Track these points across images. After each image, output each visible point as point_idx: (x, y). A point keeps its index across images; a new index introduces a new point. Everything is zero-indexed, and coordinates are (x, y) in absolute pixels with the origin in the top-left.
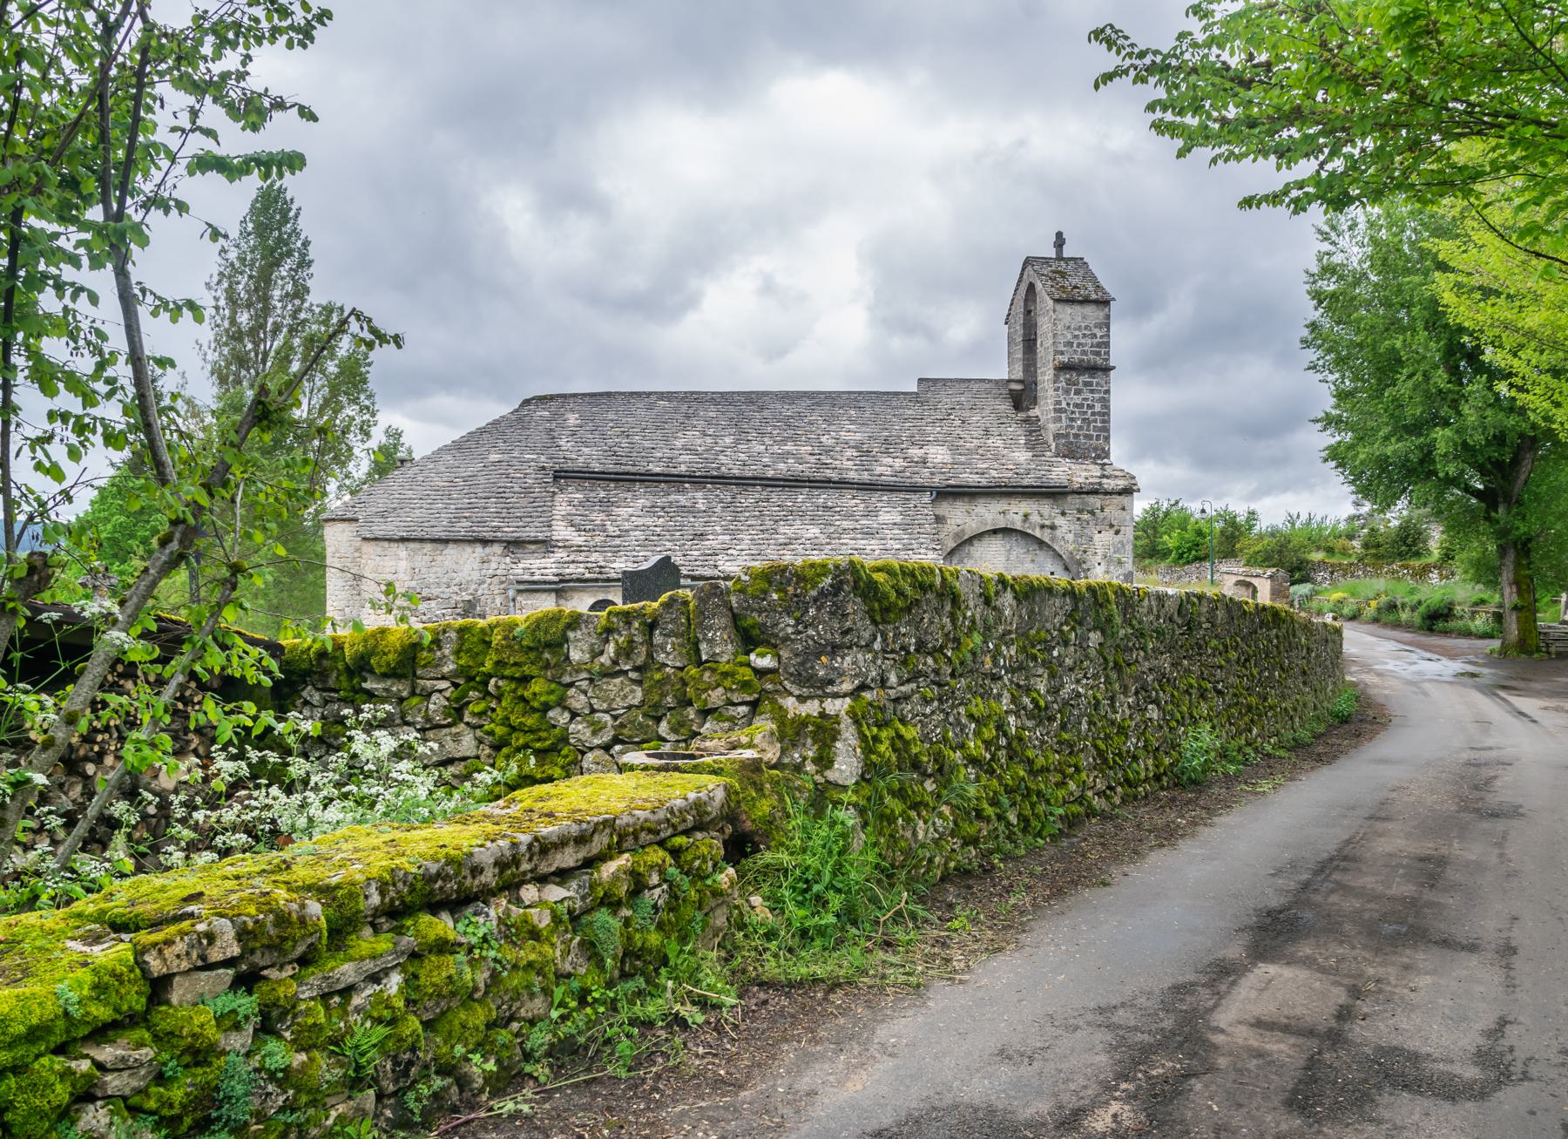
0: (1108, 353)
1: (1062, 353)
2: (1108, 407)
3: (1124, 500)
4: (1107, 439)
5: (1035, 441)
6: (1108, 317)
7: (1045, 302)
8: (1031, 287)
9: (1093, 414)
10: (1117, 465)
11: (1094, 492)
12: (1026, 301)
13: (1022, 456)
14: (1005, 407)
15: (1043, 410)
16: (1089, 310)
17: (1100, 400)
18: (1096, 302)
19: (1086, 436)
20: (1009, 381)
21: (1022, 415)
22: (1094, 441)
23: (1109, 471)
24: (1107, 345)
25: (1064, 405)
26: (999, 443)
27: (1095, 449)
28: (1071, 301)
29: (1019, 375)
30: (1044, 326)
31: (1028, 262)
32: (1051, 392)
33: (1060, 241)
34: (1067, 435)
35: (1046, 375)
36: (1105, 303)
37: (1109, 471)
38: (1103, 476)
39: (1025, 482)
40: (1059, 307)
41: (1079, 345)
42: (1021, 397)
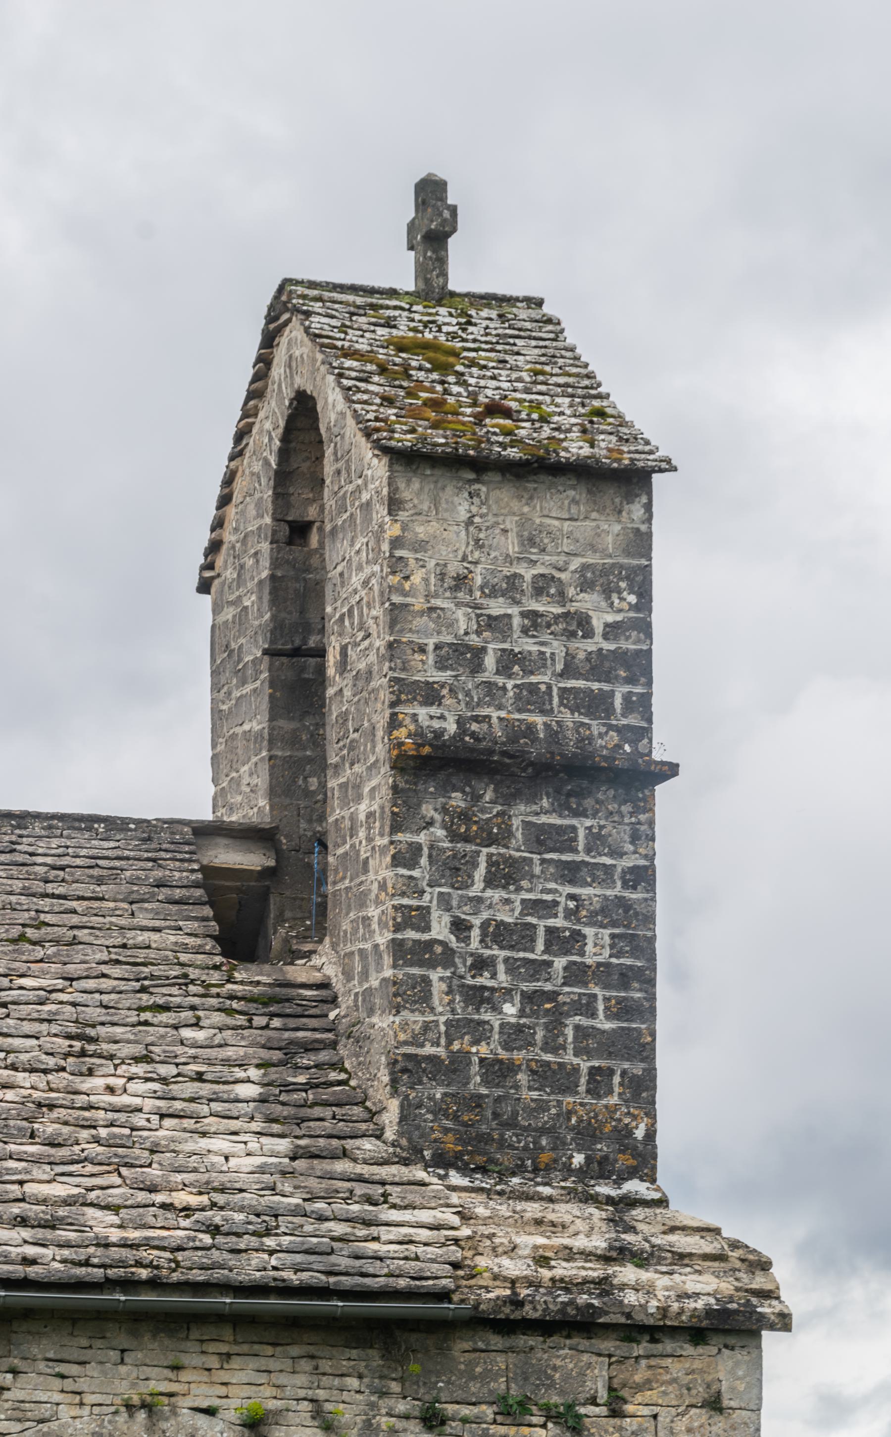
0: (642, 705)
1: (430, 695)
2: (645, 948)
3: (724, 1367)
4: (642, 1089)
5: (307, 1088)
6: (641, 542)
7: (359, 471)
8: (304, 408)
9: (577, 974)
10: (683, 1210)
11: (576, 1325)
12: (283, 478)
13: (243, 1154)
14: (180, 938)
15: (347, 962)
16: (555, 510)
17: (605, 914)
18: (585, 473)
19: (543, 1075)
20: (204, 832)
21: (253, 977)
22: (577, 1100)
23: (646, 1230)
24: (640, 666)
25: (440, 929)
26: (139, 1093)
27: (587, 1134)
28: (471, 466)
29: (254, 807)
30: (353, 569)
31: (286, 305)
32: (381, 871)
33: (433, 222)
34: (456, 1066)
35: (360, 795)
36: (625, 478)
37: (646, 1230)
38: (619, 1254)
39: (251, 1268)
40: (412, 489)
41: (508, 662)
42: (253, 899)
